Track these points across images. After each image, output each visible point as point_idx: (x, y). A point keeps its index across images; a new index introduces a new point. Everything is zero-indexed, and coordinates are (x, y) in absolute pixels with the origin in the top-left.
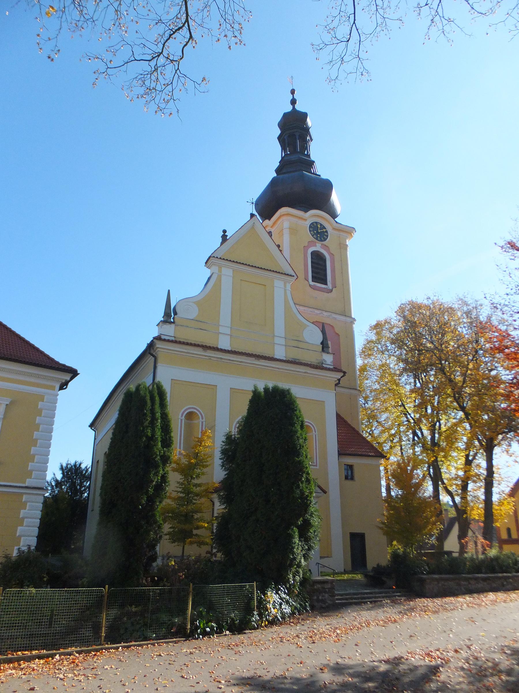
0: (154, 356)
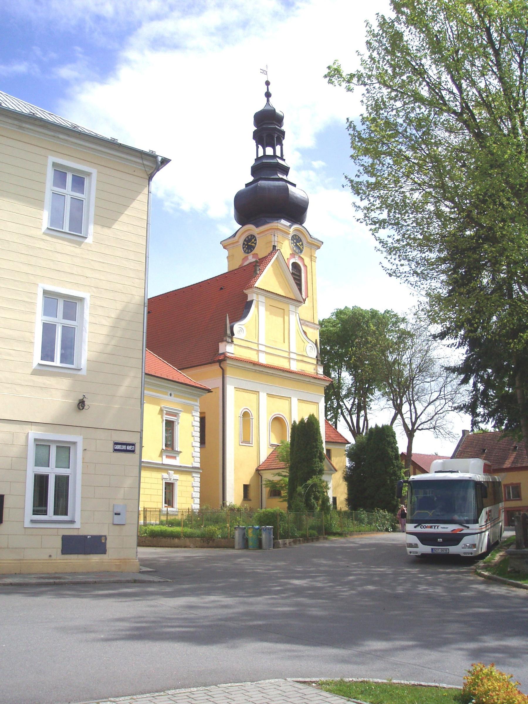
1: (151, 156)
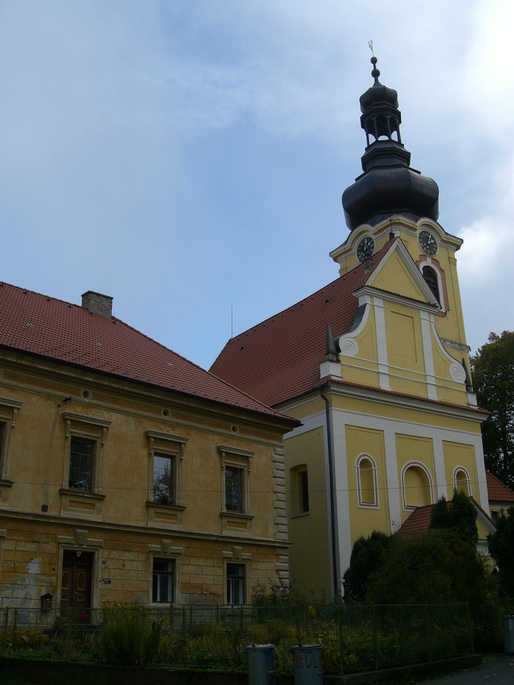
0: (326, 399)
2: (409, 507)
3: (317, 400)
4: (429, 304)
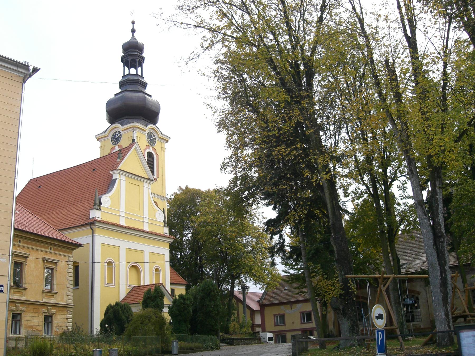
1: (25, 66)
2: (130, 286)
3: (88, 229)
4: (149, 179)
